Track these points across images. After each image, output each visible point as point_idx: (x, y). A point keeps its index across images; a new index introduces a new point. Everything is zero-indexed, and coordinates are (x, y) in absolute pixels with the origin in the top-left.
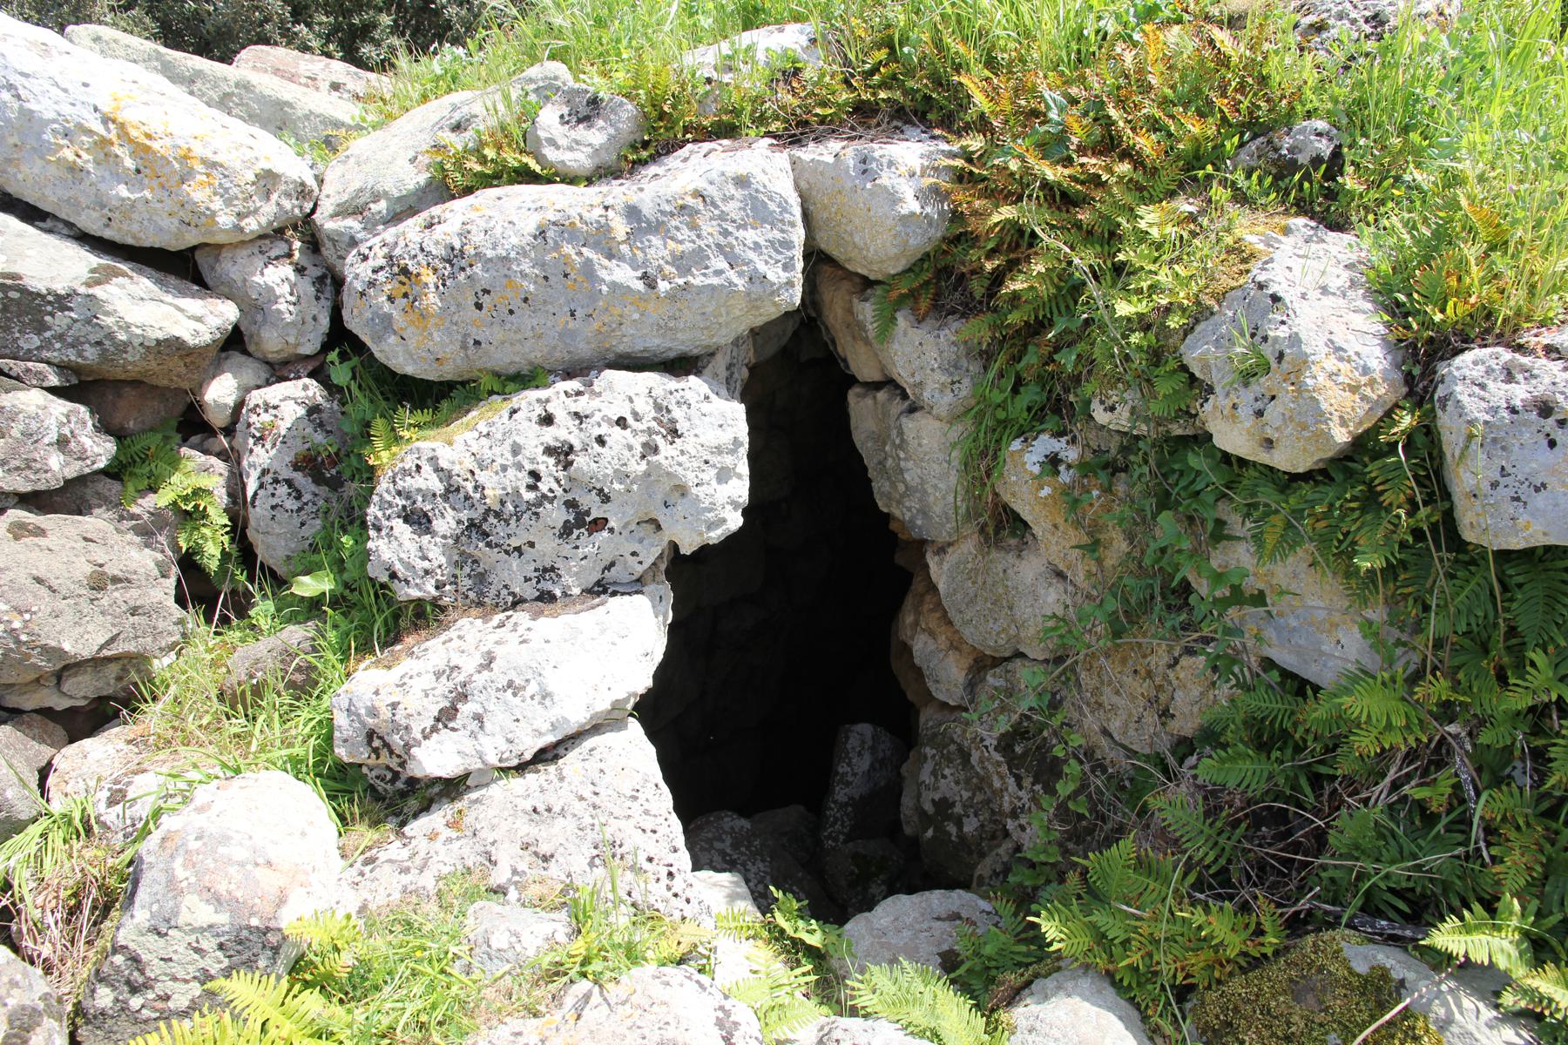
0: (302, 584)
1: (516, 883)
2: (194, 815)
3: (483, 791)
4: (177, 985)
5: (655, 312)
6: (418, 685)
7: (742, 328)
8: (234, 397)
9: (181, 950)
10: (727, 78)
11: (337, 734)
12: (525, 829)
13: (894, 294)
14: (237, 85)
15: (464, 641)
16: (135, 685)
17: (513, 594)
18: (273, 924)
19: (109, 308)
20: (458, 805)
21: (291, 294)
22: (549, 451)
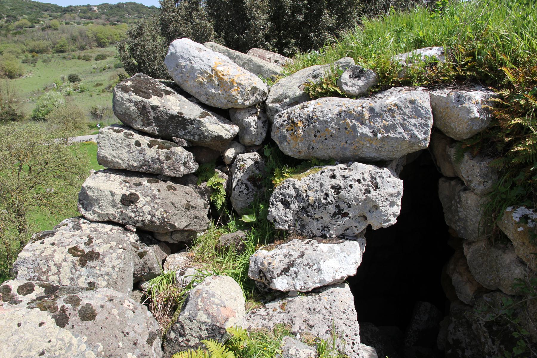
0: (245, 218)
1: (300, 333)
2: (205, 286)
3: (293, 298)
4: (193, 338)
5: (375, 144)
6: (278, 258)
7: (405, 153)
9: (196, 327)
10: (409, 65)
11: (250, 269)
12: (305, 314)
13: (464, 146)
14: (248, 60)
15: (295, 246)
16: (192, 240)
17: (313, 234)
18: (223, 327)
19: (204, 125)
20: (284, 301)
22: (333, 187)
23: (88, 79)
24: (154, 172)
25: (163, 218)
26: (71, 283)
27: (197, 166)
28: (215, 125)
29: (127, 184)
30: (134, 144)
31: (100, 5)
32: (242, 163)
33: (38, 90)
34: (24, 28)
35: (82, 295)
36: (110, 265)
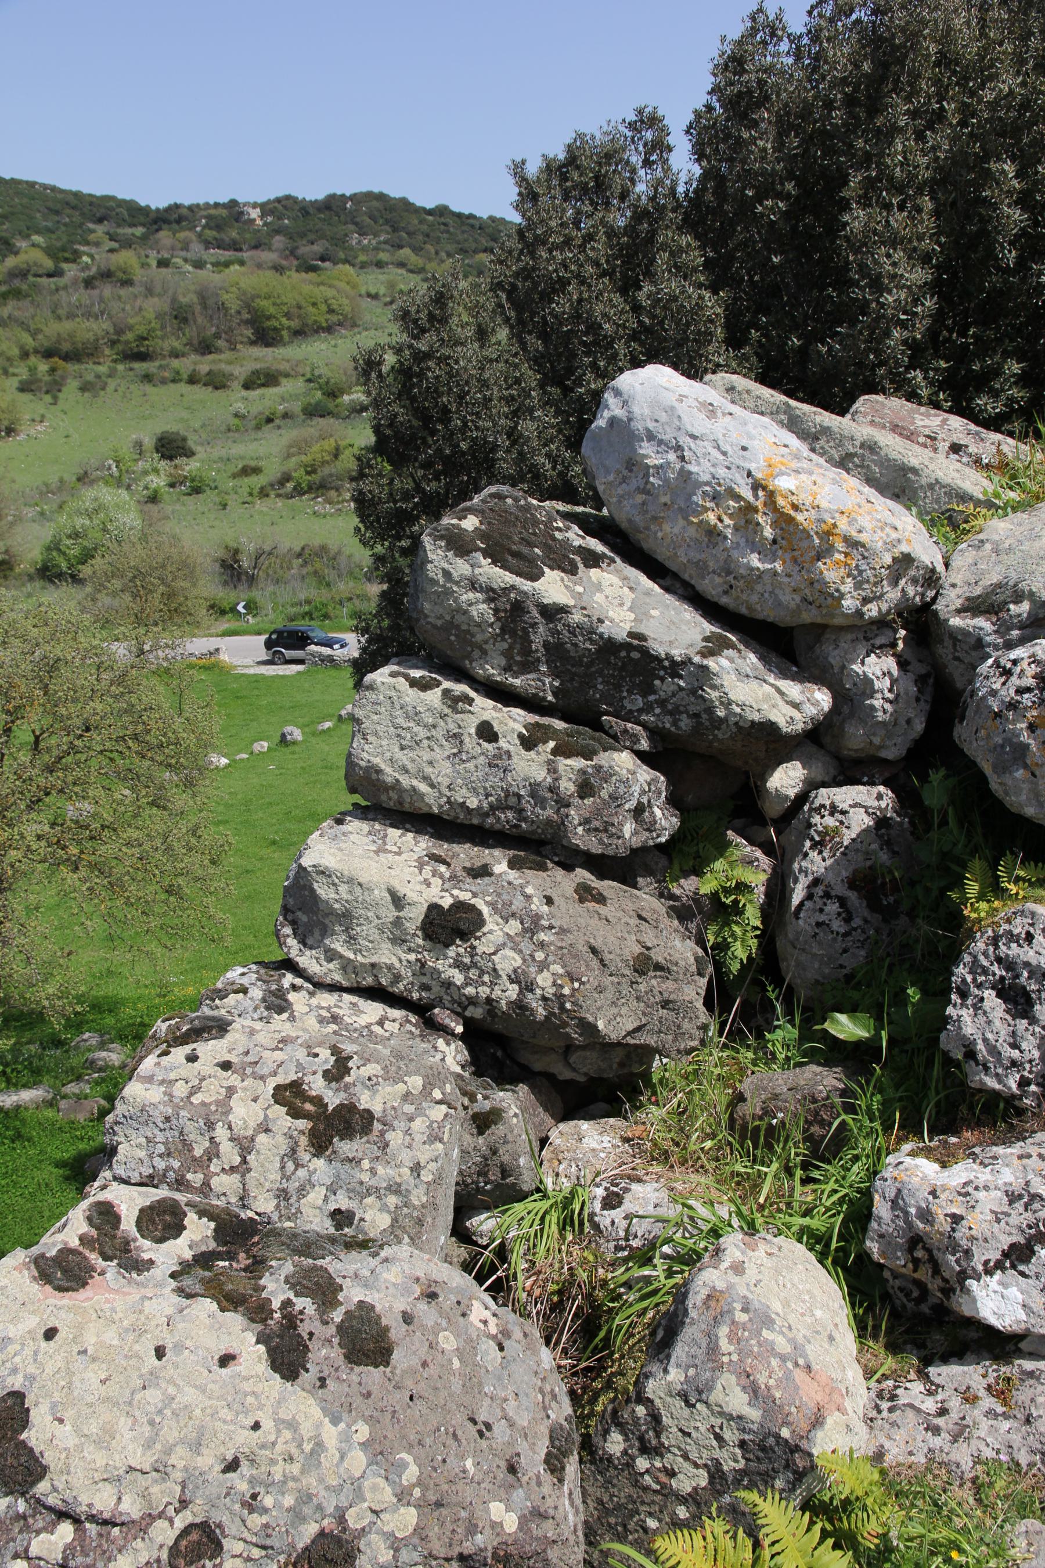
4: (686, 1465)
8: (796, 790)
9: (703, 1429)
11: (874, 1225)
18: (804, 1444)
21: (890, 691)
23: (218, 452)
24: (534, 832)
25: (560, 997)
26: (278, 1206)
27: (674, 820)
28: (754, 684)
29: (443, 868)
30: (473, 731)
31: (269, 202)
32: (830, 822)
33: (61, 481)
34: (31, 279)
35: (338, 1265)
36: (406, 1157)
